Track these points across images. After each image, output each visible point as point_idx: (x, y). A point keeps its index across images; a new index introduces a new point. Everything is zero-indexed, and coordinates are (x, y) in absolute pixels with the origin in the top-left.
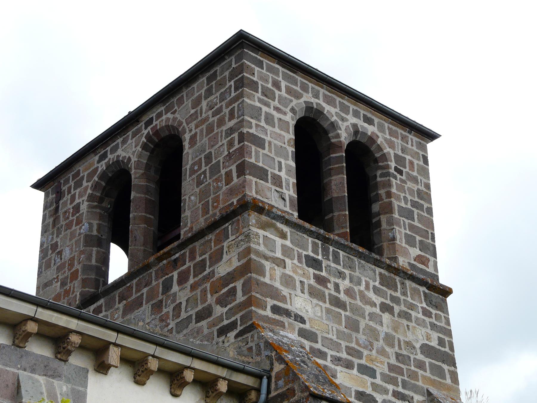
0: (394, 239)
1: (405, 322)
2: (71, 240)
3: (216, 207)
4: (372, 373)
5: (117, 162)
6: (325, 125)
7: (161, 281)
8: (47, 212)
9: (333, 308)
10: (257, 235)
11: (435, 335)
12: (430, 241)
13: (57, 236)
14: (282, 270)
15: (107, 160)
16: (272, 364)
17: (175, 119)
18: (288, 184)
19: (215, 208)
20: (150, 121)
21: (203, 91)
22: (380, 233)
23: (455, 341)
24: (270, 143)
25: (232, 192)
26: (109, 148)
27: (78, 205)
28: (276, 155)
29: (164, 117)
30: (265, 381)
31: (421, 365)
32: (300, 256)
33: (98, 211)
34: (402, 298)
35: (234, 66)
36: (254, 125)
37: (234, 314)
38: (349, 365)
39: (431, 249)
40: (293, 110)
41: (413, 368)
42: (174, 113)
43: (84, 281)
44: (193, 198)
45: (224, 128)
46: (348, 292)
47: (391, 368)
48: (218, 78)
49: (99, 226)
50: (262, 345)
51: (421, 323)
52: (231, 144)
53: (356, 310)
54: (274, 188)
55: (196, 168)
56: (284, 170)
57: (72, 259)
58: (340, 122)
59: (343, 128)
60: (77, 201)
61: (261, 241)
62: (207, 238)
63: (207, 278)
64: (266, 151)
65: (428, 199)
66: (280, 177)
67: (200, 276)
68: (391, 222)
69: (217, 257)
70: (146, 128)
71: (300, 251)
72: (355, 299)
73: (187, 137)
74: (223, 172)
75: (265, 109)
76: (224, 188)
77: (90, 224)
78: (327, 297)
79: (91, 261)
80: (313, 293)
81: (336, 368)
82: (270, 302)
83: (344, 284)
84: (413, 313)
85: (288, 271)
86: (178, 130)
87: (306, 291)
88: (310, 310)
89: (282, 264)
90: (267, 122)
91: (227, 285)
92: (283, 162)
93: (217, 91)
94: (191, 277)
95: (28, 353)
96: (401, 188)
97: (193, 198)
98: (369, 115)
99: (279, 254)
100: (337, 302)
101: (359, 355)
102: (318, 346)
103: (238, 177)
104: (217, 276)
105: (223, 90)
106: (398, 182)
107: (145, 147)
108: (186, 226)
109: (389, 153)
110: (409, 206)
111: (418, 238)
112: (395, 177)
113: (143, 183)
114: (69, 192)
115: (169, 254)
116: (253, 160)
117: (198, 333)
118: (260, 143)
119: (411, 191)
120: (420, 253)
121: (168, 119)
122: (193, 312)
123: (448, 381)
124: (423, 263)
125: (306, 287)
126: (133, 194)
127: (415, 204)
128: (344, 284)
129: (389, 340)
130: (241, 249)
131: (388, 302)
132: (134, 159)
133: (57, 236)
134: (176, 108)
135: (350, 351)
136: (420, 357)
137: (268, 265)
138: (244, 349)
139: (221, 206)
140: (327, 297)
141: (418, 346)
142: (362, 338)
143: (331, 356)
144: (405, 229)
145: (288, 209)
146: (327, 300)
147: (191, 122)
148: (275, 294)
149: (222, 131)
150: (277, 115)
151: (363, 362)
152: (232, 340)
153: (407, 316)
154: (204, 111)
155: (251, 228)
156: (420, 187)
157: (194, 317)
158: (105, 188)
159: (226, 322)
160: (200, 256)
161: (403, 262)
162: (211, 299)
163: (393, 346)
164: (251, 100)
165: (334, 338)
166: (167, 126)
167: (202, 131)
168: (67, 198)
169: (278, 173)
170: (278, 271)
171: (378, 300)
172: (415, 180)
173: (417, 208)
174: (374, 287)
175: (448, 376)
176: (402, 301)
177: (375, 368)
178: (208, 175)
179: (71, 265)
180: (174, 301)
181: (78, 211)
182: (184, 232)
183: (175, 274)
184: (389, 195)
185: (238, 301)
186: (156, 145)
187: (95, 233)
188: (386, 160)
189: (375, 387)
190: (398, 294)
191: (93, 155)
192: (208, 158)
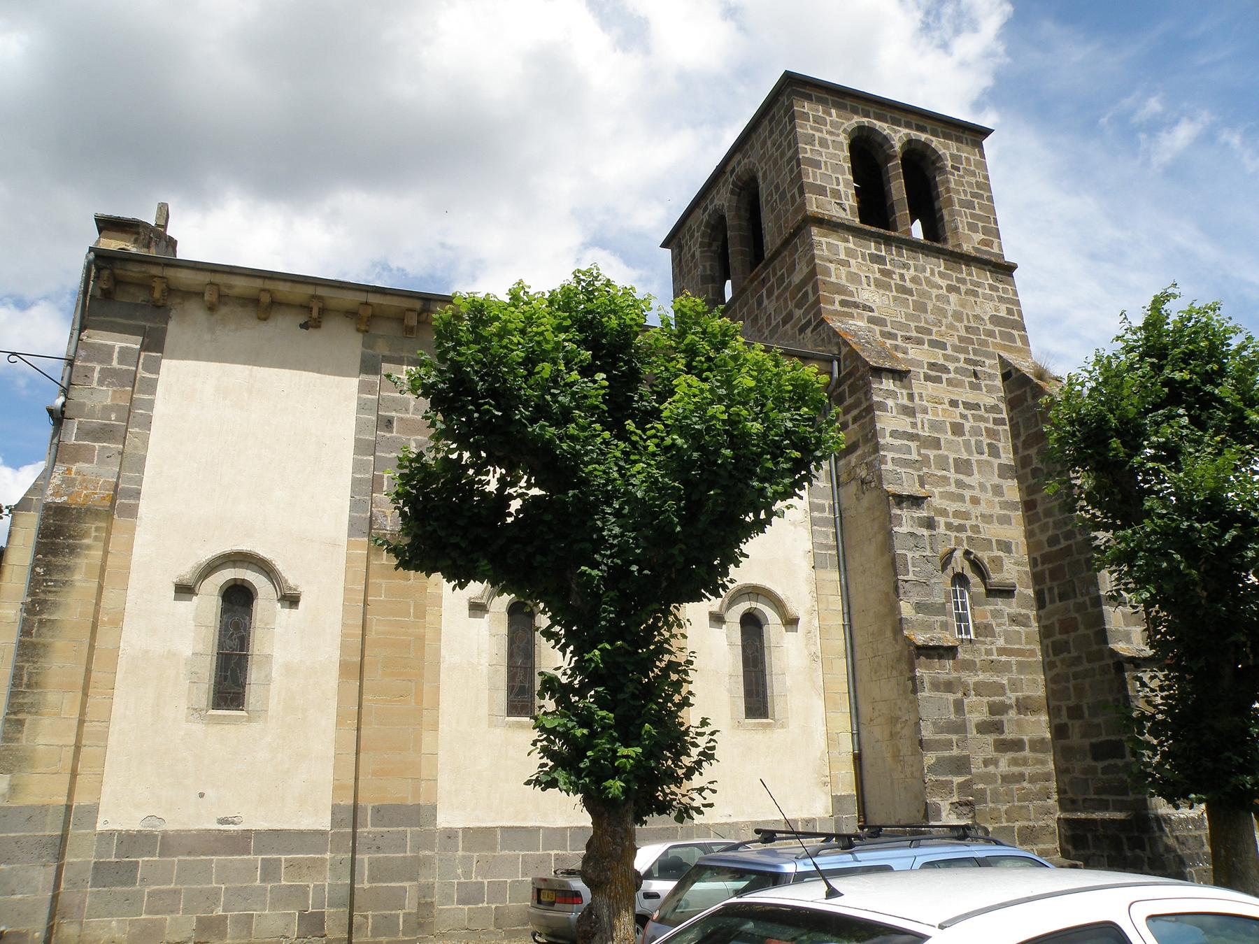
0: (957, 228)
1: (972, 299)
4: (943, 346)
5: (716, 210)
6: (879, 139)
7: (755, 299)
9: (900, 295)
10: (820, 243)
12: (993, 225)
14: (847, 269)
16: (840, 348)
17: (750, 162)
18: (847, 196)
19: (786, 228)
23: (1024, 309)
24: (826, 162)
25: (797, 211)
27: (694, 252)
28: (833, 172)
30: (836, 363)
31: (991, 334)
32: (863, 255)
33: (709, 254)
34: (968, 278)
35: (786, 104)
36: (809, 151)
37: (809, 313)
38: (920, 342)
39: (995, 231)
40: (845, 131)
41: (983, 337)
42: (749, 157)
44: (770, 224)
45: (785, 159)
46: (913, 280)
47: (961, 339)
49: (711, 265)
50: (831, 334)
51: (991, 298)
52: (791, 171)
53: (923, 294)
54: (833, 201)
56: (842, 184)
58: (893, 135)
61: (824, 247)
63: (786, 288)
64: (823, 170)
65: (988, 188)
66: (839, 191)
67: (782, 288)
68: (952, 214)
69: (792, 269)
71: (864, 251)
72: (921, 284)
73: (760, 174)
74: (788, 196)
75: (817, 134)
76: (791, 209)
77: (704, 266)
78: (893, 287)
80: (879, 285)
81: (907, 345)
82: (838, 298)
83: (909, 274)
84: (980, 290)
85: (854, 269)
87: (872, 284)
88: (877, 300)
89: (846, 264)
90: (821, 145)
92: (840, 177)
93: (777, 129)
97: (770, 224)
98: (921, 123)
99: (842, 256)
101: (929, 332)
102: (888, 329)
104: (793, 285)
106: (956, 178)
107: (732, 192)
109: (944, 154)
110: (969, 197)
111: (980, 224)
114: (687, 244)
115: (757, 275)
116: (811, 180)
118: (816, 164)
119: (971, 185)
120: (984, 237)
122: (779, 319)
123: (1019, 344)
124: (986, 245)
125: (872, 280)
127: (974, 195)
128: (909, 274)
129: (958, 316)
131: (954, 283)
135: (919, 330)
136: (990, 327)
137: (832, 266)
138: (819, 340)
139: (790, 225)
140: (893, 287)
141: (986, 318)
142: (931, 317)
143: (902, 336)
144: (967, 218)
145: (849, 217)
146: (894, 289)
148: (841, 290)
151: (933, 337)
152: (809, 335)
153: (975, 294)
155: (813, 237)
156: (978, 179)
158: (711, 234)
161: (966, 248)
163: (961, 321)
164: (803, 129)
165: (903, 320)
168: (686, 249)
169: (837, 187)
170: (843, 270)
171: (944, 283)
173: (977, 198)
174: (940, 273)
175: (1018, 340)
176: (968, 281)
177: (945, 341)
180: (766, 313)
182: (767, 254)
184: (948, 190)
186: (741, 189)
187: (708, 272)
188: (942, 160)
189: (946, 357)
192: (777, 187)
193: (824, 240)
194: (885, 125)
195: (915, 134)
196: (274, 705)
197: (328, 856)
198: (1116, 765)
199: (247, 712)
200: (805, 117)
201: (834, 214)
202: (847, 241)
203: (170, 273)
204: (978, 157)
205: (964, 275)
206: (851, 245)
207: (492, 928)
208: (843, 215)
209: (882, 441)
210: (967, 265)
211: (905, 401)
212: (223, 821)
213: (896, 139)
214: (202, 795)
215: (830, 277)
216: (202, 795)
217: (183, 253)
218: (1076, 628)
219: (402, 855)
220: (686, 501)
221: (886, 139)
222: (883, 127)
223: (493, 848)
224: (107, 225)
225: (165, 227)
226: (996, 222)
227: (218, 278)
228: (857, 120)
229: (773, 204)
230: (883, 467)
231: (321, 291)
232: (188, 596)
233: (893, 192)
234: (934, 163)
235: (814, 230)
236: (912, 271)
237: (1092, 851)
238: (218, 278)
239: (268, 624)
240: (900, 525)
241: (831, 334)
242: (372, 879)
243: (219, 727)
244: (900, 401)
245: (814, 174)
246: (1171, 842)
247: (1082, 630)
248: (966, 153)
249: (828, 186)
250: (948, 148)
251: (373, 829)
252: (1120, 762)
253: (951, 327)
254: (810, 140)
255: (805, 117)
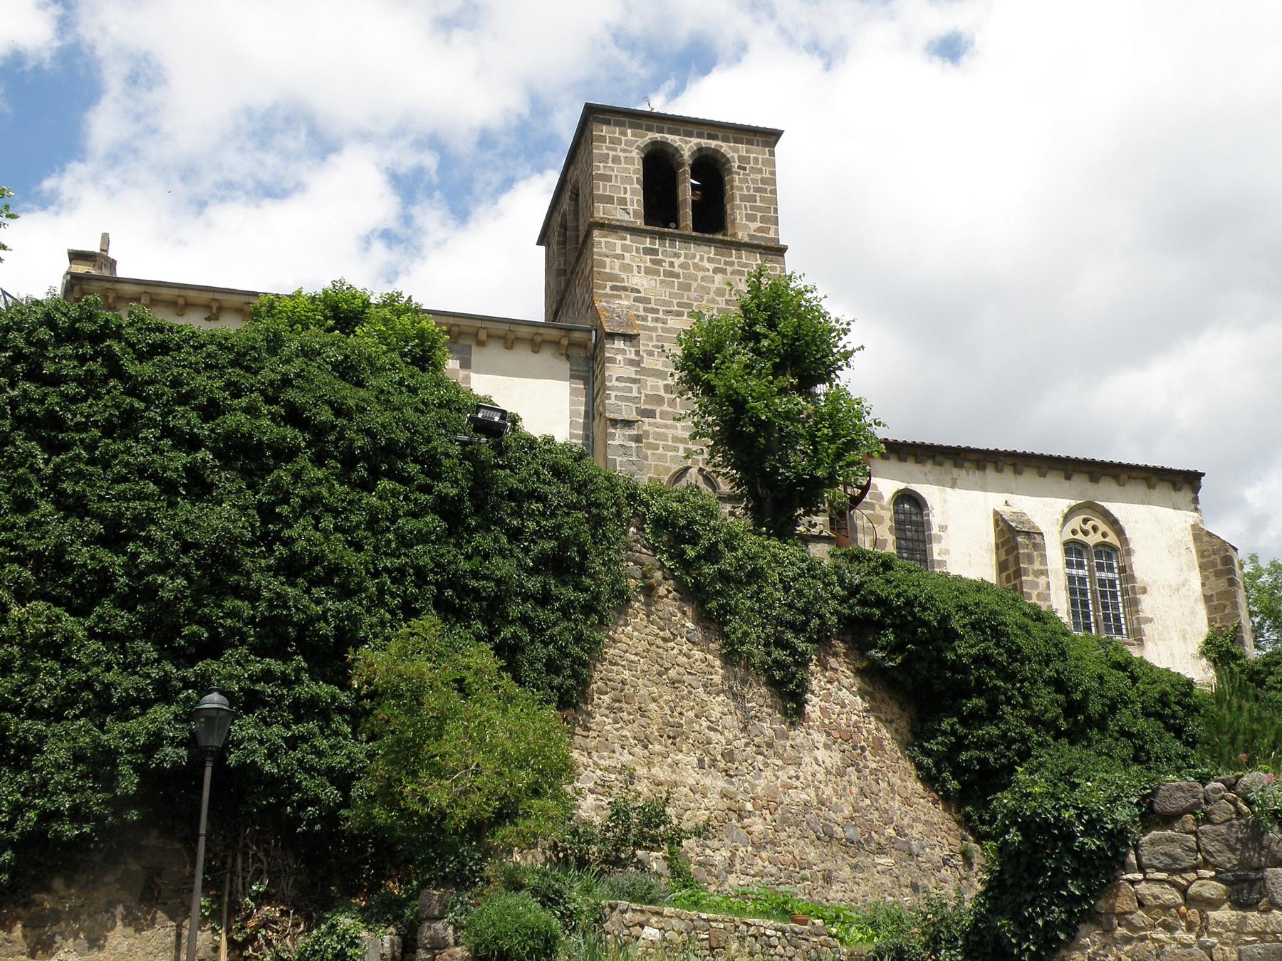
0: (735, 219)
6: (671, 151)
24: (616, 176)
32: (638, 250)
38: (680, 314)
40: (638, 147)
56: (629, 193)
75: (612, 153)
82: (609, 284)
87: (642, 272)
90: (614, 162)
92: (628, 187)
98: (713, 133)
99: (619, 251)
102: (652, 305)
109: (733, 157)
119: (755, 181)
125: (642, 269)
128: (677, 262)
131: (722, 266)
135: (679, 305)
137: (608, 260)
145: (632, 219)
161: (742, 236)
165: (667, 298)
170: (617, 263)
171: (711, 266)
193: (603, 240)
194: (677, 138)
195: (705, 142)
200: (603, 139)
201: (619, 218)
202: (625, 239)
203: (119, 286)
204: (767, 156)
205: (733, 259)
206: (628, 242)
208: (626, 218)
209: (608, 384)
211: (633, 356)
213: (686, 149)
215: (605, 268)
217: (120, 273)
222: (674, 139)
224: (75, 256)
225: (106, 251)
226: (776, 211)
227: (150, 289)
230: (607, 401)
231: (218, 296)
234: (724, 165)
235: (596, 233)
236: (682, 259)
238: (150, 289)
240: (614, 440)
244: (628, 356)
245: (605, 187)
248: (756, 153)
249: (616, 196)
253: (713, 301)
254: (604, 158)
255: (603, 139)
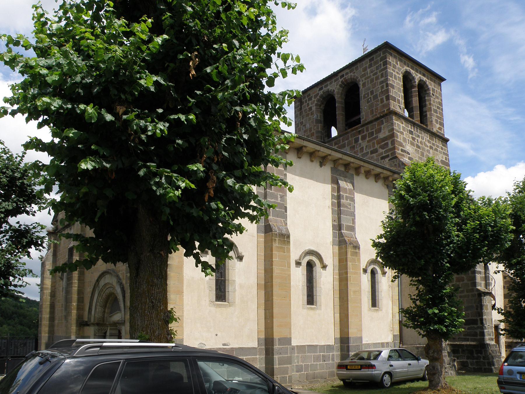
0: (432, 121)
1: (436, 152)
2: (309, 121)
3: (377, 112)
6: (411, 78)
7: (353, 138)
8: (296, 109)
10: (395, 123)
11: (444, 156)
13: (303, 119)
15: (323, 90)
17: (354, 76)
19: (376, 112)
20: (343, 76)
21: (368, 65)
22: (427, 119)
25: (384, 106)
26: (323, 86)
29: (349, 74)
33: (319, 110)
35: (382, 55)
42: (354, 73)
43: (317, 137)
45: (379, 81)
46: (421, 143)
48: (375, 60)
49: (320, 115)
50: (401, 164)
51: (441, 152)
52: (382, 87)
54: (398, 104)
55: (366, 96)
57: (310, 129)
59: (417, 79)
60: (310, 106)
62: (373, 123)
63: (375, 138)
64: (395, 90)
67: (371, 138)
68: (431, 115)
69: (379, 131)
70: (341, 78)
73: (361, 83)
74: (379, 98)
77: (317, 115)
79: (318, 129)
80: (412, 144)
82: (400, 148)
86: (356, 80)
90: (395, 79)
91: (384, 141)
94: (367, 138)
95: (339, 170)
96: (434, 102)
100: (418, 147)
103: (386, 101)
104: (379, 138)
105: (377, 65)
107: (341, 86)
108: (363, 118)
111: (439, 120)
112: (432, 97)
113: (340, 100)
114: (306, 102)
116: (391, 94)
117: (372, 158)
119: (437, 102)
121: (351, 76)
122: (369, 151)
126: (337, 105)
128: (420, 140)
130: (390, 128)
131: (431, 145)
132: (336, 91)
133: (303, 119)
134: (355, 71)
139: (379, 111)
147: (363, 77)
149: (378, 82)
150: (397, 75)
153: (436, 150)
154: (368, 73)
157: (370, 152)
159: (384, 155)
160: (371, 130)
161: (435, 130)
162: (376, 146)
166: (351, 78)
167: (368, 81)
168: (305, 104)
171: (429, 145)
172: (438, 98)
178: (372, 99)
179: (310, 130)
181: (311, 110)
183: (360, 137)
184: (430, 104)
185: (389, 148)
187: (319, 118)
190: (434, 142)
191: (316, 88)
192: (372, 92)
193: (396, 122)
196: (237, 301)
197: (258, 356)
198: (474, 327)
199: (229, 303)
207: (305, 380)
210: (435, 138)
212: (224, 345)
214: (216, 335)
216: (216, 335)
218: (463, 281)
219: (287, 355)
220: (59, 180)
221: (414, 78)
223: (305, 353)
228: (406, 68)
229: (369, 99)
232: (205, 255)
233: (413, 102)
234: (426, 91)
235: (394, 118)
237: (461, 354)
239: (233, 268)
241: (401, 164)
242: (279, 364)
243: (220, 309)
246: (490, 352)
247: (466, 281)
250: (431, 85)
251: (278, 347)
252: (475, 326)
